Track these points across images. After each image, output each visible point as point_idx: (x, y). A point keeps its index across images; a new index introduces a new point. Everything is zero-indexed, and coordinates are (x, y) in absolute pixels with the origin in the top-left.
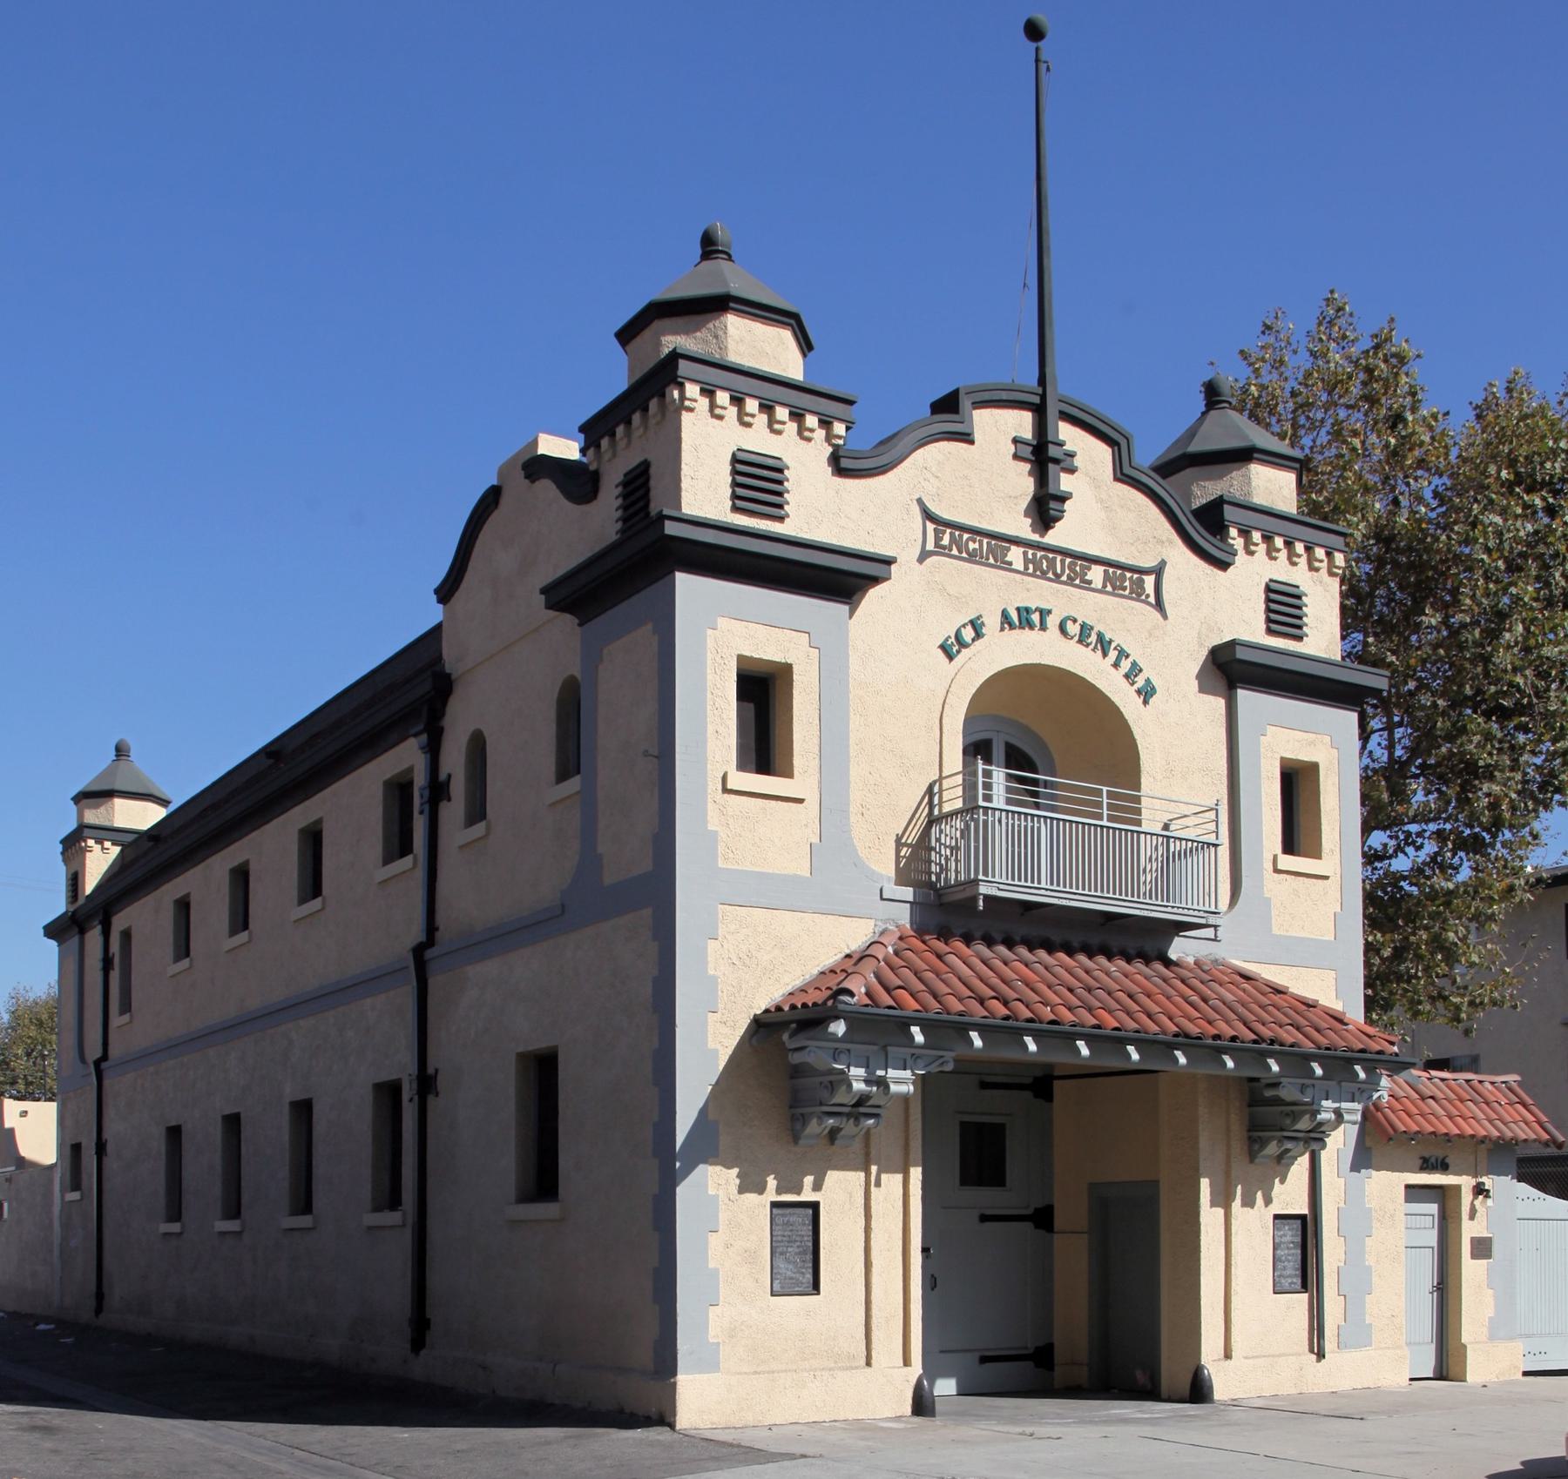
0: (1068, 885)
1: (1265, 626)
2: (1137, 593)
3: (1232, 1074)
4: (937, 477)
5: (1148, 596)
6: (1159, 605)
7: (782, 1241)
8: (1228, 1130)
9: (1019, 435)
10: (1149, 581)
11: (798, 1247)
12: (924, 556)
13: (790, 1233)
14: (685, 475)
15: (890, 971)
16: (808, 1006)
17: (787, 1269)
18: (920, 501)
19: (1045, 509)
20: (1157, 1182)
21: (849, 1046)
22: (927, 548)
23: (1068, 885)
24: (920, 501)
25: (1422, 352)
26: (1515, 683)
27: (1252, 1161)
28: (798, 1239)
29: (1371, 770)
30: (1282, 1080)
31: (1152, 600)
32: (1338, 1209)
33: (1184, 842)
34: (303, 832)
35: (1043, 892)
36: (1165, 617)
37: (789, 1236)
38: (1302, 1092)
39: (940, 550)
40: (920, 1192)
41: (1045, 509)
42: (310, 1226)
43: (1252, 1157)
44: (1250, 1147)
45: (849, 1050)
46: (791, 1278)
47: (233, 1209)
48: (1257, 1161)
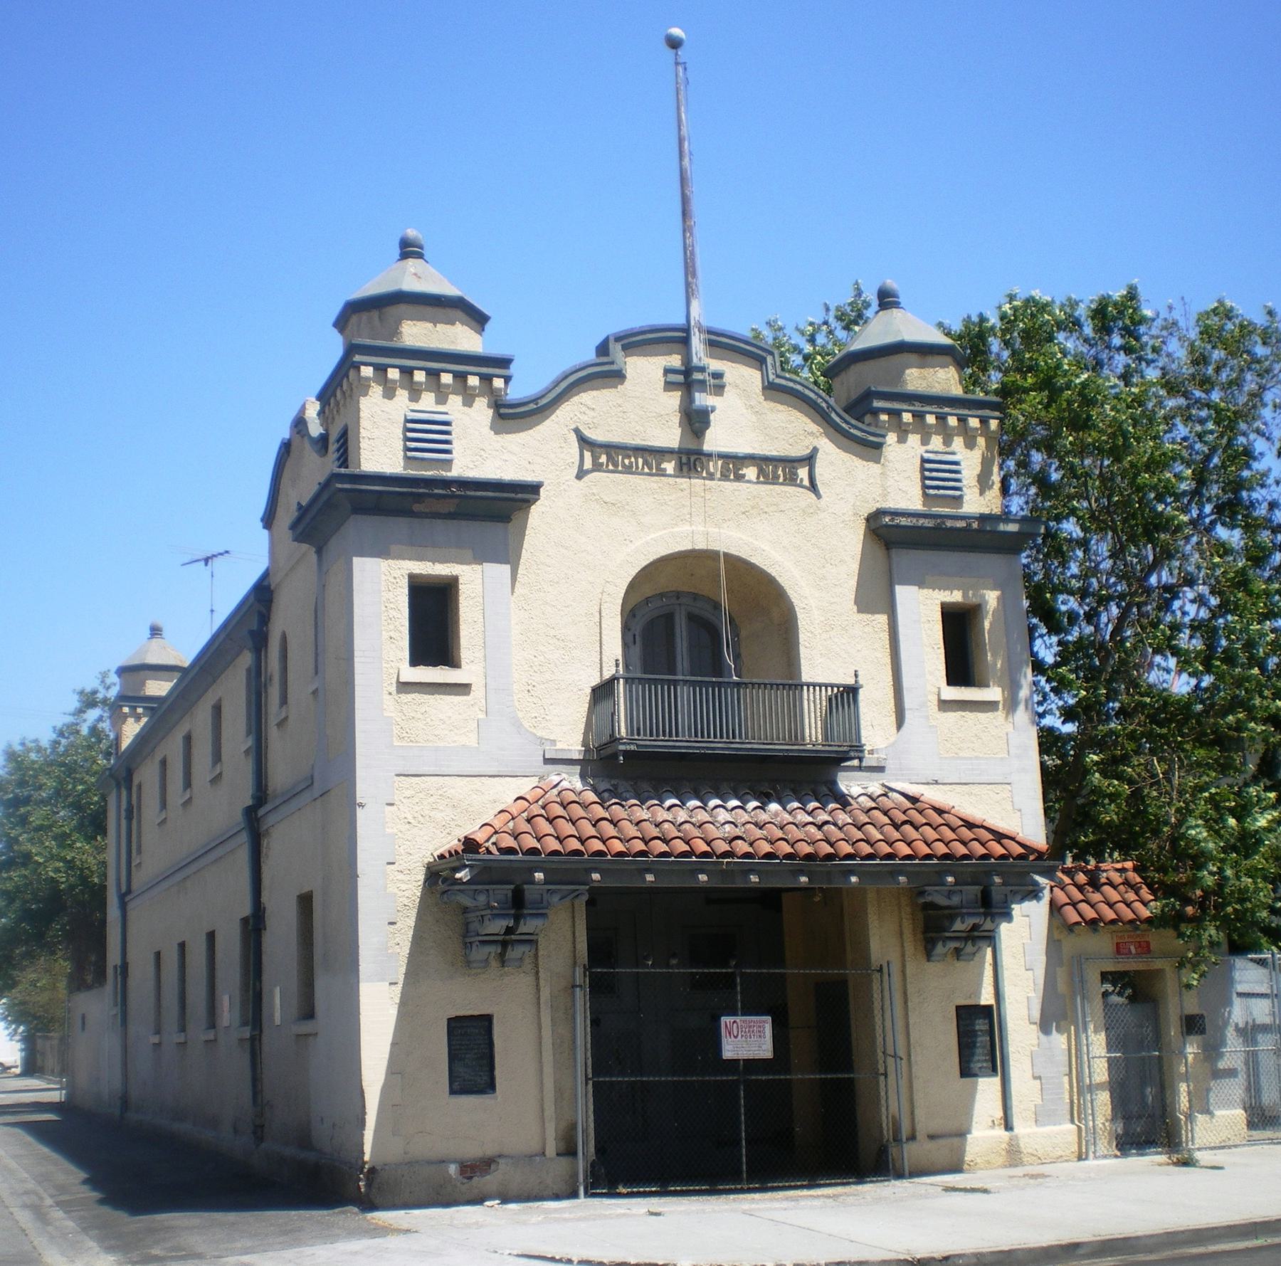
0: (680, 735)
1: (921, 492)
2: (792, 480)
3: (705, 885)
4: (593, 409)
5: (802, 480)
6: (813, 487)
7: (460, 1049)
8: (901, 934)
9: (669, 364)
10: (803, 473)
11: (476, 1054)
12: (581, 474)
13: (467, 1043)
14: (364, 438)
15: (981, 847)
16: (445, 857)
17: (465, 1073)
18: (577, 431)
19: (696, 421)
20: (847, 981)
21: (959, 888)
22: (585, 468)
23: (700, 735)
24: (577, 431)
25: (1170, 301)
26: (1142, 485)
27: (958, 959)
28: (476, 1047)
29: (368, 379)
30: (927, 888)
31: (806, 483)
32: (1028, 998)
33: (829, 689)
34: (160, 761)
35: (660, 743)
36: (819, 496)
37: (467, 1045)
38: (949, 898)
39: (597, 467)
40: (1044, 958)
41: (696, 421)
42: (183, 1041)
43: (929, 955)
44: (926, 948)
45: (487, 890)
46: (471, 1080)
47: (183, 1029)
48: (933, 958)
